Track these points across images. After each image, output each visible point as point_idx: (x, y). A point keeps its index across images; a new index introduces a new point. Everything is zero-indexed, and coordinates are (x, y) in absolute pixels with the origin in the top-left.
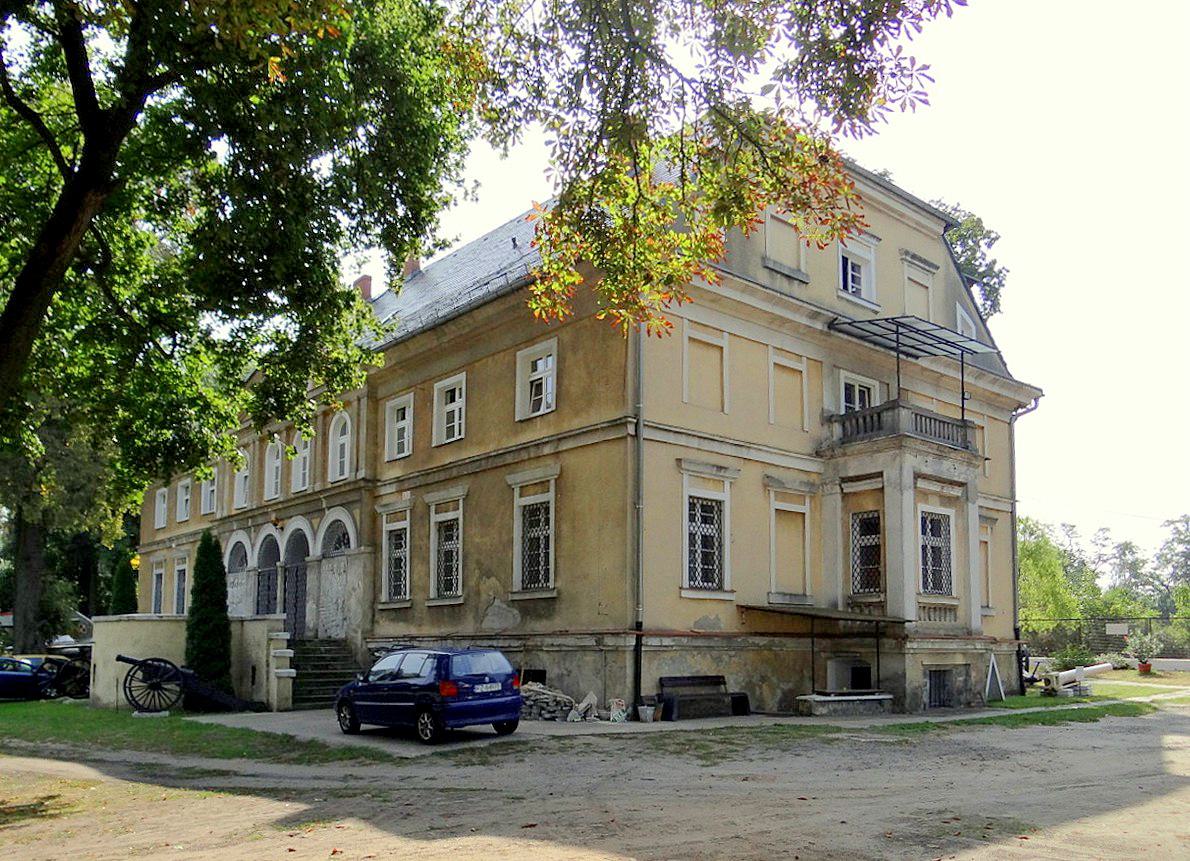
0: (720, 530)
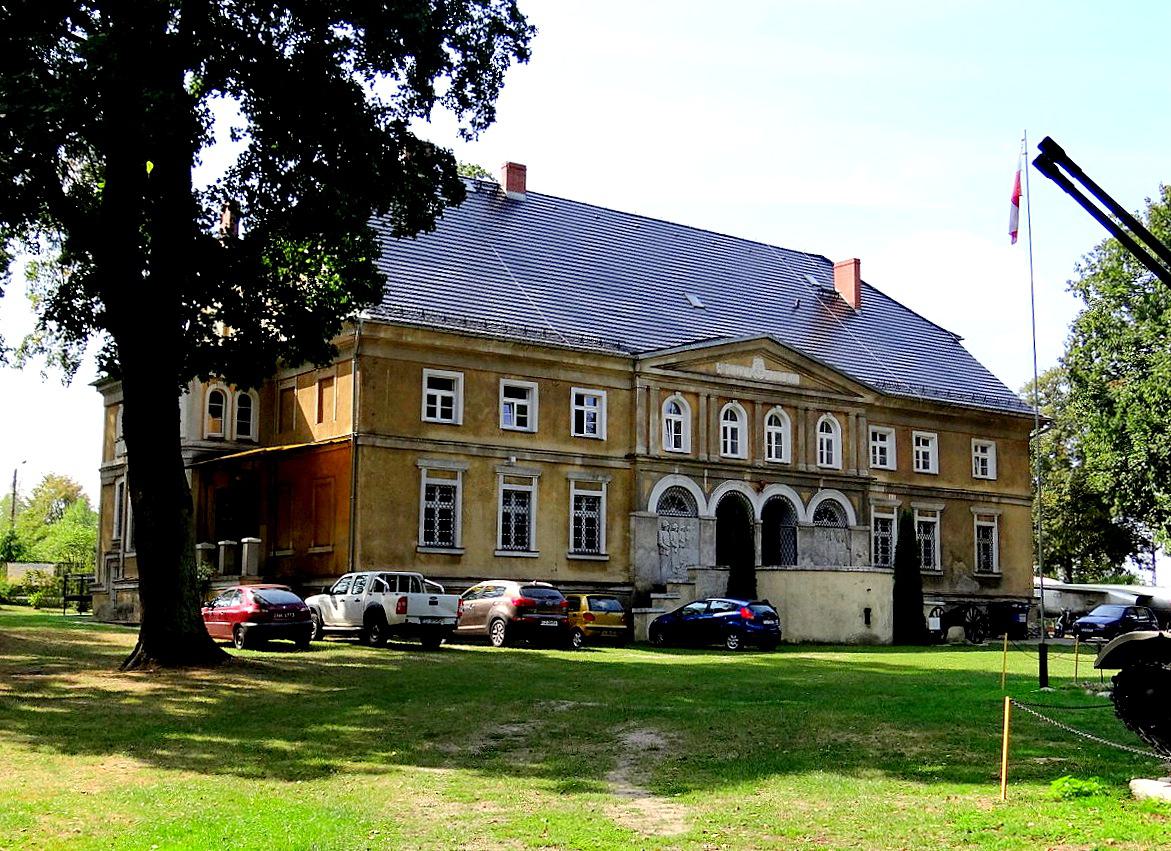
0: (599, 514)
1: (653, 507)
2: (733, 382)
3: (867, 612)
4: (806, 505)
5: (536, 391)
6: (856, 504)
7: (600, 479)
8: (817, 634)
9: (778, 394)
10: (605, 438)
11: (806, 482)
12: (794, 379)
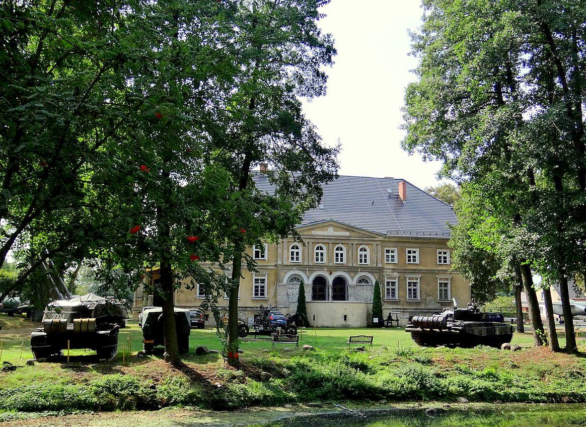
1: (285, 282)
2: (318, 237)
3: (345, 317)
4: (308, 278)
5: (397, 250)
6: (376, 277)
7: (264, 273)
8: (326, 325)
9: (337, 240)
10: (267, 259)
11: (352, 270)
12: (347, 234)
